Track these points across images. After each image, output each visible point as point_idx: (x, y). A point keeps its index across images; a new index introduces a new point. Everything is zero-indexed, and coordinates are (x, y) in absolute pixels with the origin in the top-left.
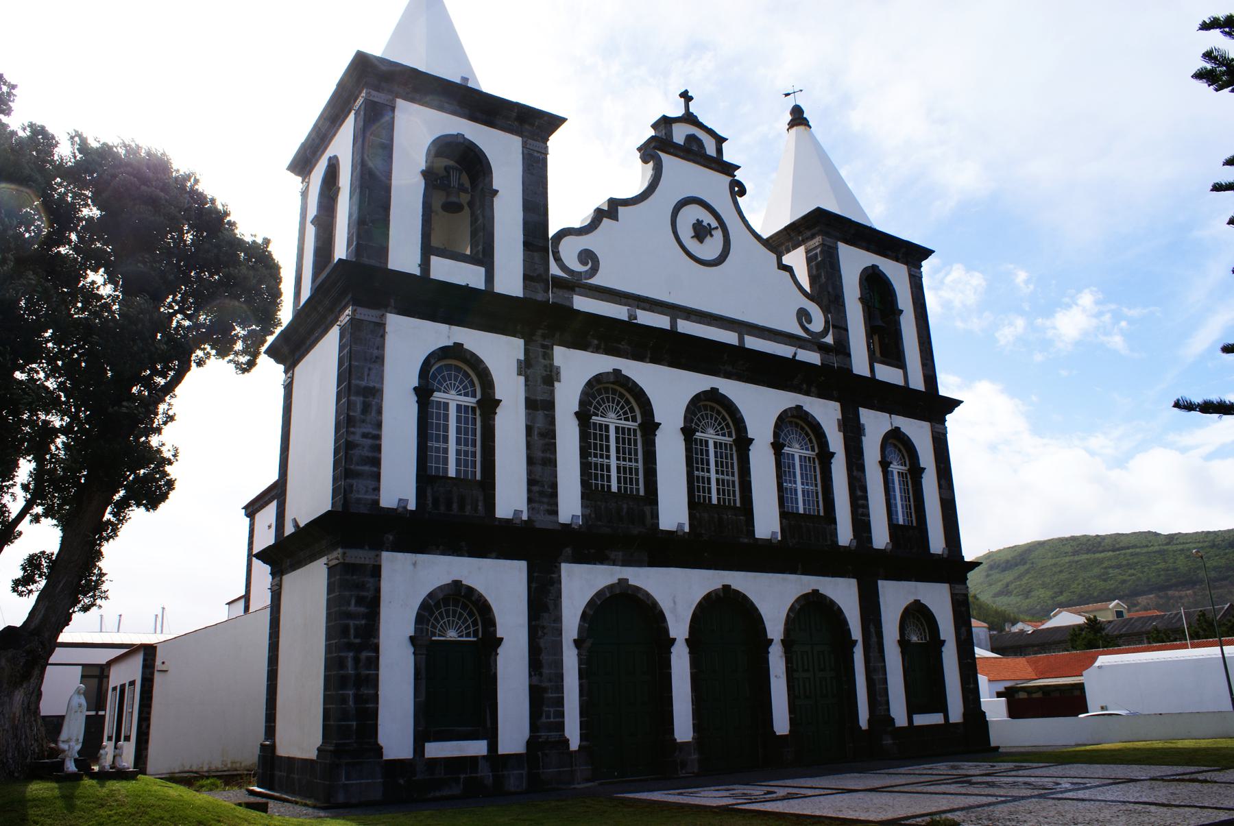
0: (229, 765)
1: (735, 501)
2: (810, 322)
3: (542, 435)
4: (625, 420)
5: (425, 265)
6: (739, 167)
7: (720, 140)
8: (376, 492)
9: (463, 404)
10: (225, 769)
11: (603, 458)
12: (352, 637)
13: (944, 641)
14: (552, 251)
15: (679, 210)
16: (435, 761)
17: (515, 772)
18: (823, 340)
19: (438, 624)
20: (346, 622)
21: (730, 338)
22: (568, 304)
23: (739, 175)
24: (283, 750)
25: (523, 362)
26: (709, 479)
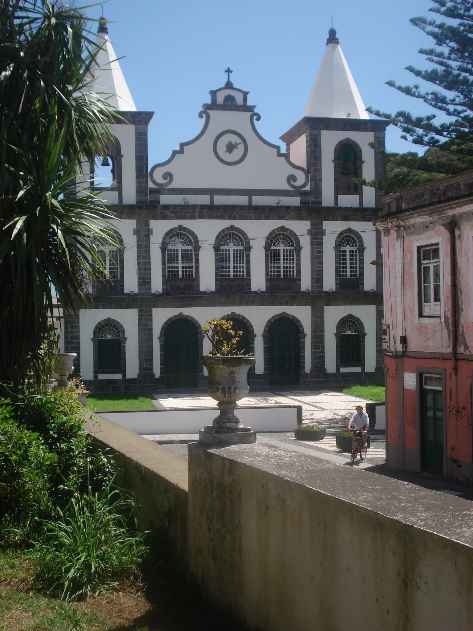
3: (144, 258)
6: (255, 106)
7: (245, 94)
9: (352, 250)
13: (366, 334)
23: (256, 110)
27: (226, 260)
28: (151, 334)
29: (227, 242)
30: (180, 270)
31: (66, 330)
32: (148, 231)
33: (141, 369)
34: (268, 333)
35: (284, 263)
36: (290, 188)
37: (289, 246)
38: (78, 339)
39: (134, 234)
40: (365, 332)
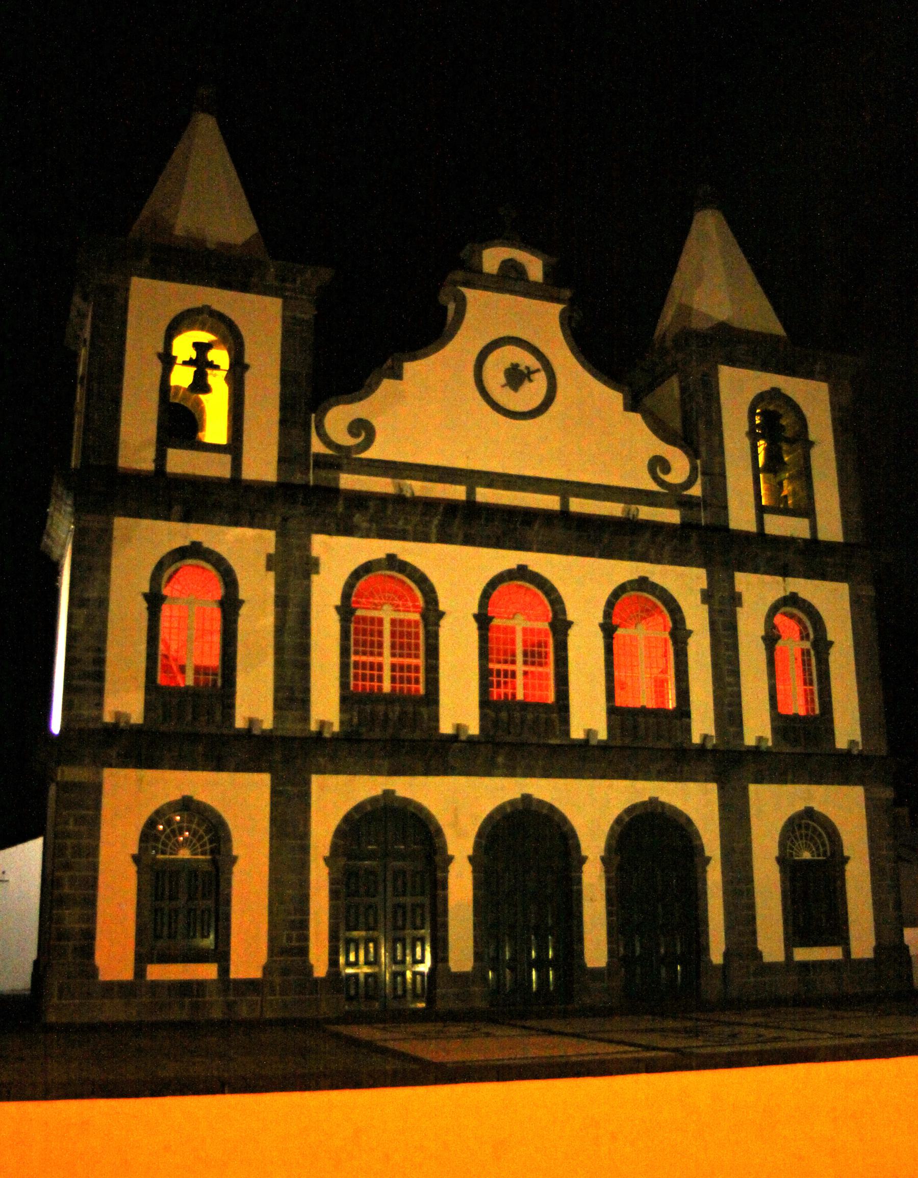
2: (667, 469)
5: (161, 458)
16: (156, 985)
18: (685, 493)
21: (551, 502)
22: (333, 485)
28: (305, 851)
30: (387, 674)
31: (440, 875)
36: (655, 487)
39: (269, 568)
40: (846, 853)
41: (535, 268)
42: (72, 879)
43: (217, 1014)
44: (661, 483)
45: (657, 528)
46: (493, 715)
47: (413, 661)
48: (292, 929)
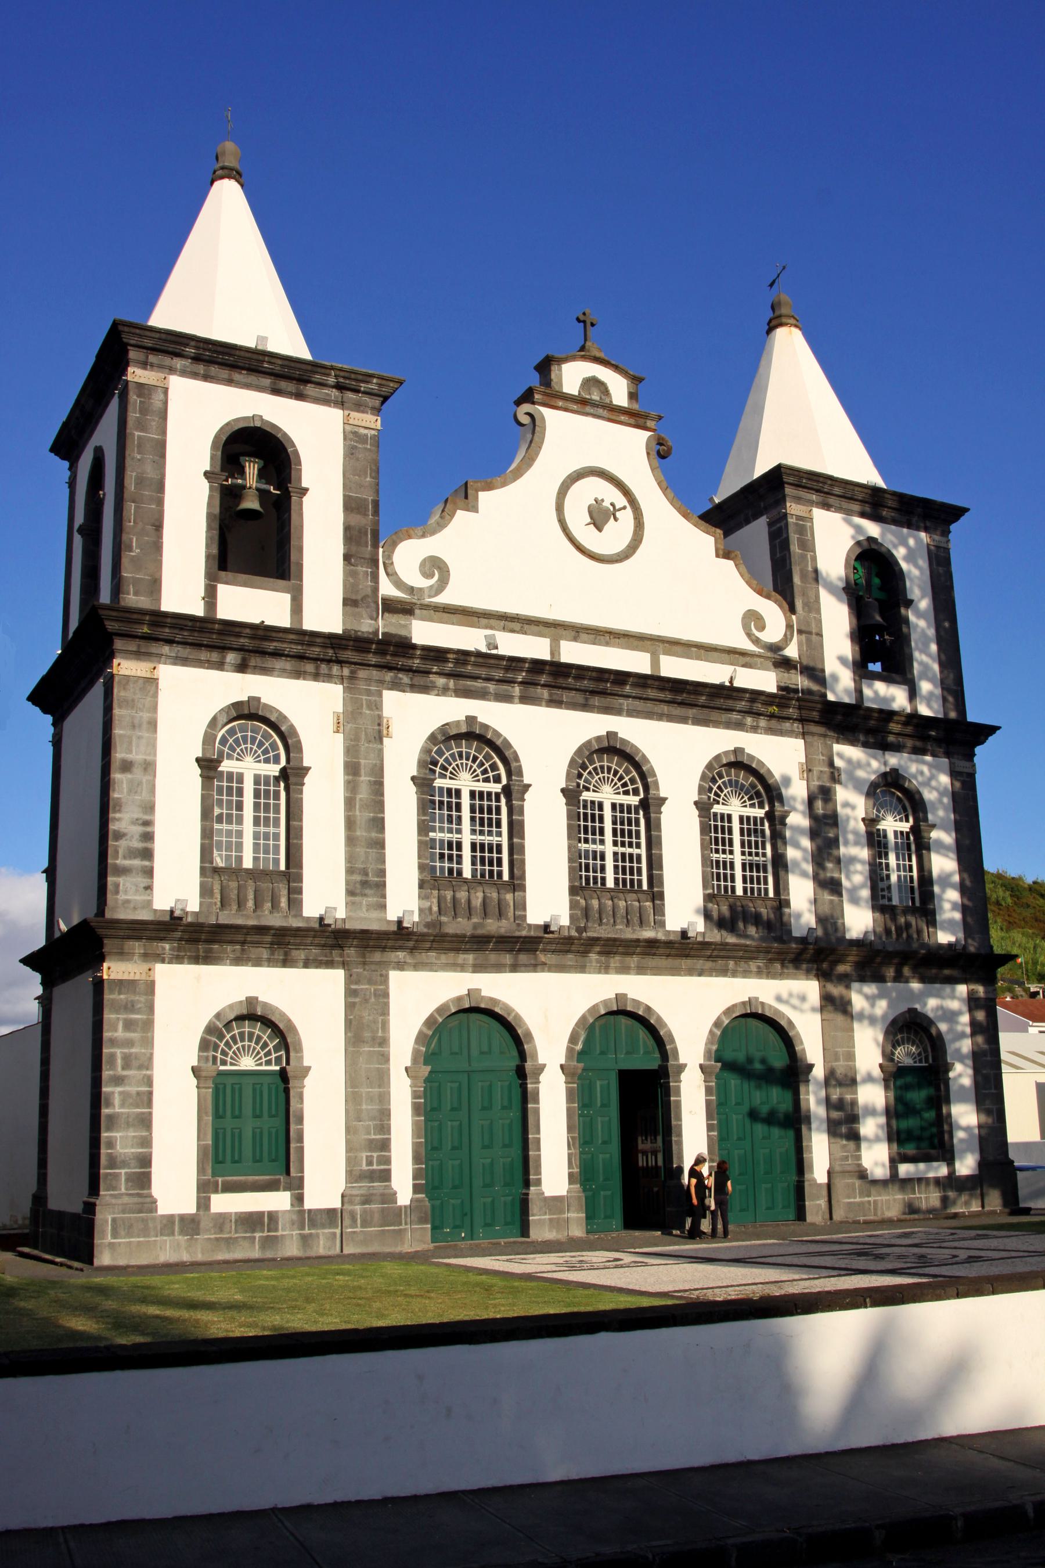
0: (20, 1222)
1: (766, 890)
2: (762, 627)
4: (483, 781)
5: (211, 597)
8: (149, 891)
10: (16, 1226)
11: (444, 832)
12: (119, 1069)
14: (384, 563)
15: (568, 488)
17: (326, 1231)
19: (230, 1050)
20: (112, 1050)
24: (54, 1203)
25: (341, 716)
26: (732, 864)
27: (490, 825)
29: (475, 766)
32: (379, 725)
33: (353, 1175)
34: (716, 1061)
35: (743, 853)
37: (487, 780)
38: (147, 1069)
41: (619, 391)
42: (125, 1095)
43: (292, 1249)
44: (756, 641)
45: (756, 695)
46: (583, 902)
47: (635, 851)
48: (371, 1150)
